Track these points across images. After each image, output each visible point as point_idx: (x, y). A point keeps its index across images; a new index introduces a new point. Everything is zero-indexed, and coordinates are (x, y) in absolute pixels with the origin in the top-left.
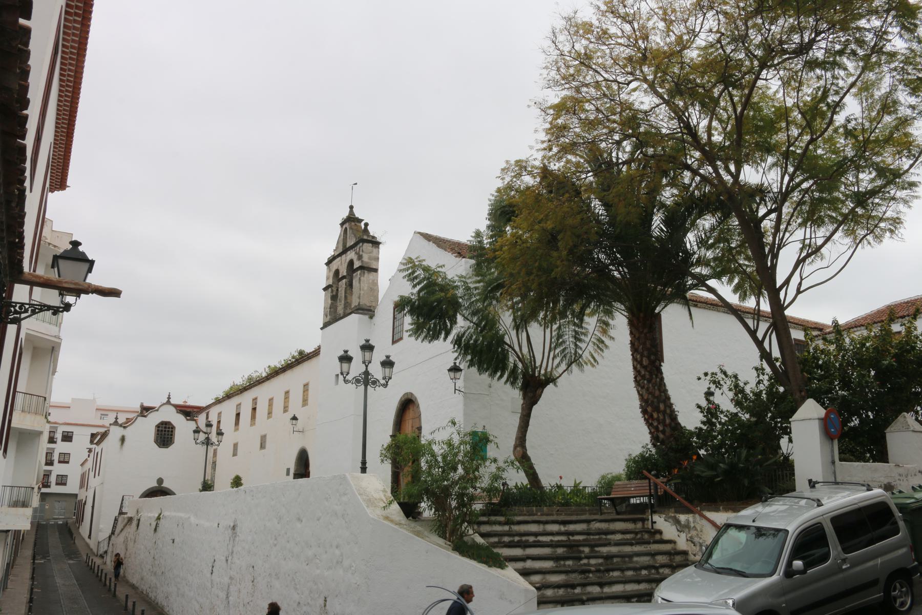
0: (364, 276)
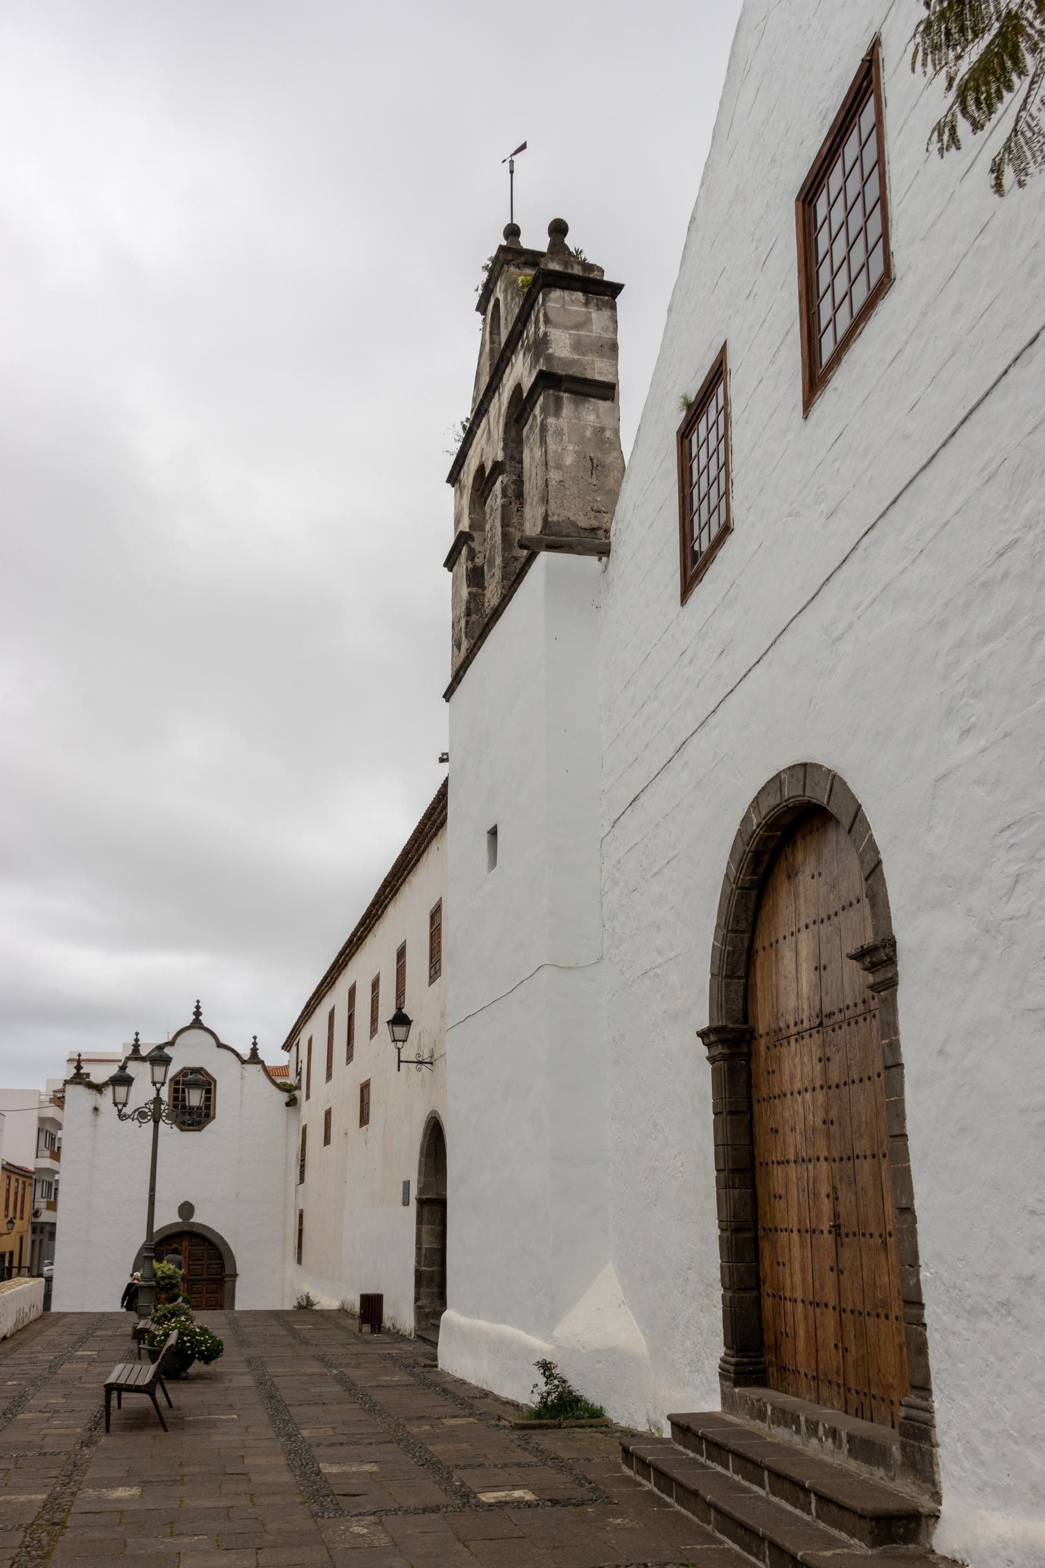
0: (557, 414)
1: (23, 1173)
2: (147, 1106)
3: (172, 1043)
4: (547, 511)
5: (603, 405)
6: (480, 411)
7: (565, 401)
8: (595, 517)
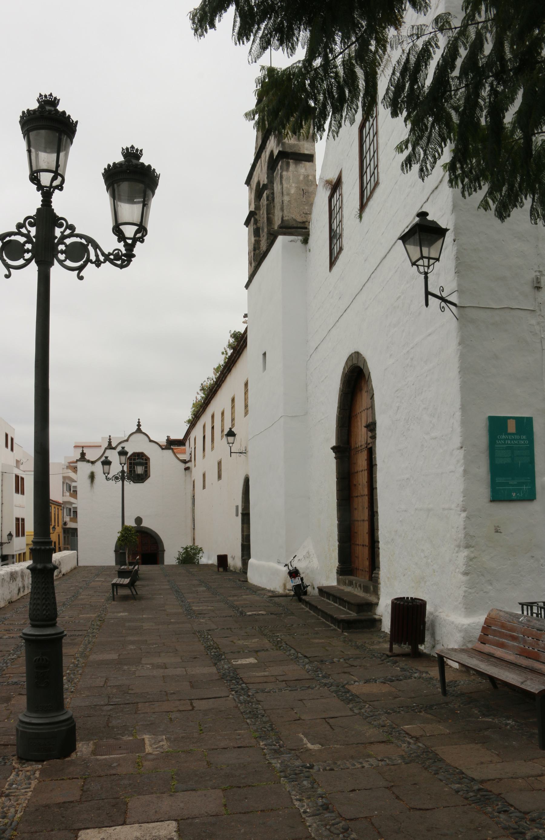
0: (287, 170)
1: (57, 504)
2: (24, 230)
3: (127, 440)
4: (283, 215)
5: (308, 164)
6: (258, 156)
7: (291, 163)
8: (305, 216)
